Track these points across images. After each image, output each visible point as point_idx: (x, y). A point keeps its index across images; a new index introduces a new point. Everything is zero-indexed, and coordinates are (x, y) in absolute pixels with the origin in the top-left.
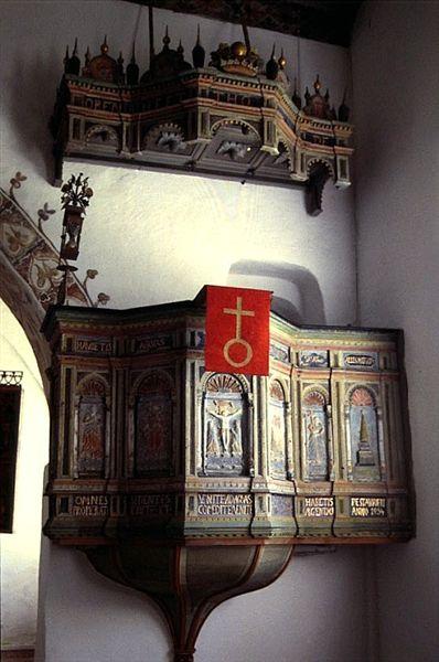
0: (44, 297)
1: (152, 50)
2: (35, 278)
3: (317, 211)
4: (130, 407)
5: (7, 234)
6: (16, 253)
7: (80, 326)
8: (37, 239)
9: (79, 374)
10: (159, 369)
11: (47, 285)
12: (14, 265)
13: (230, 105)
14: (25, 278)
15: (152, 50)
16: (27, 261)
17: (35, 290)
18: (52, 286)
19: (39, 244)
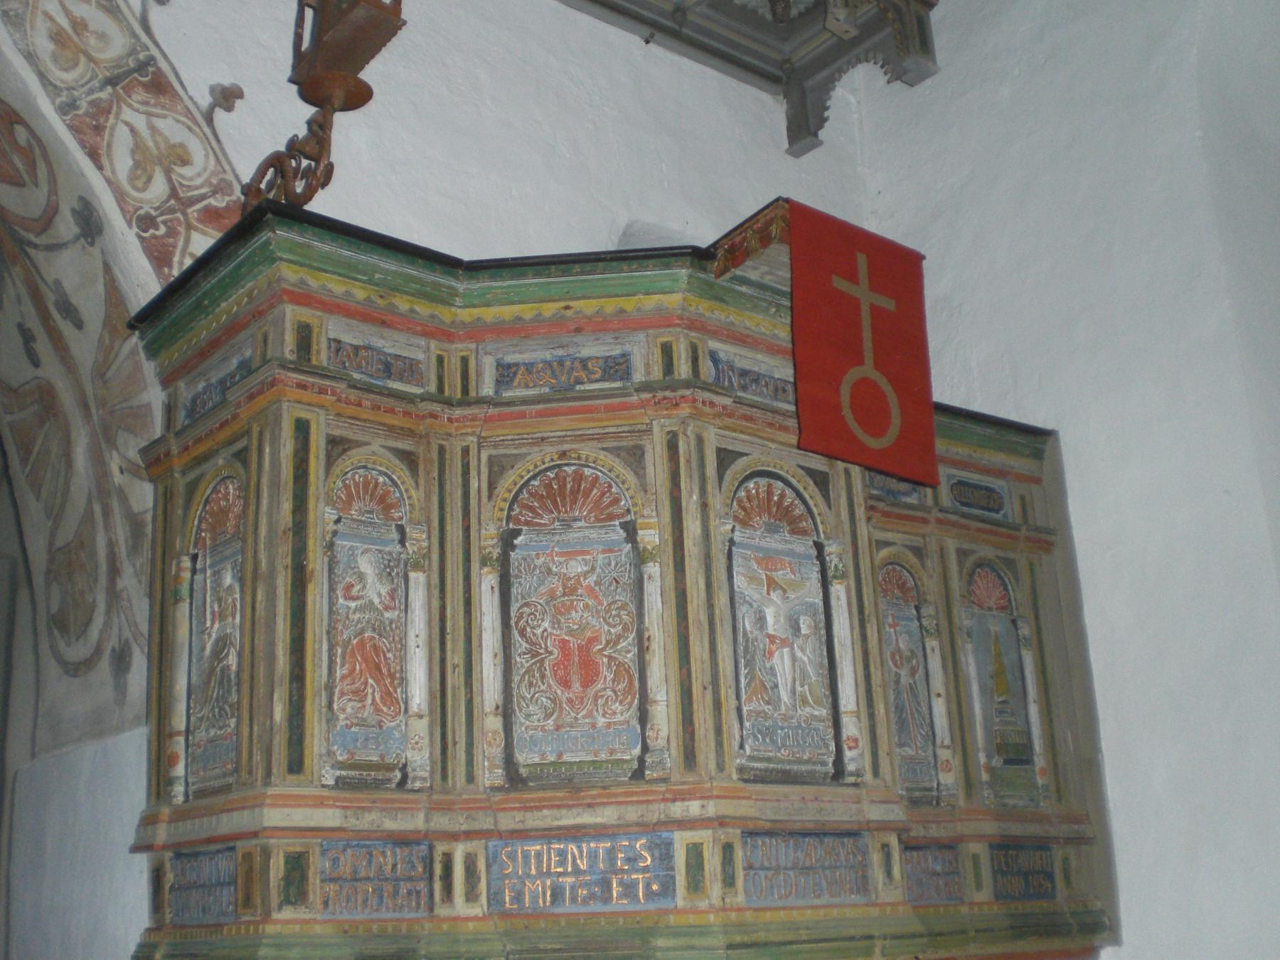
0: (146, 222)
1: (791, 446)
2: (122, 162)
3: (809, 140)
4: (484, 562)
5: (48, 16)
6: (70, 77)
7: (360, 294)
8: (132, 52)
9: (333, 442)
10: (587, 450)
11: (159, 188)
12: (63, 110)
13: (541, 794)
14: (94, 155)
15: (791, 446)
16: (101, 110)
17: (120, 197)
18: (174, 193)
19: (142, 67)
